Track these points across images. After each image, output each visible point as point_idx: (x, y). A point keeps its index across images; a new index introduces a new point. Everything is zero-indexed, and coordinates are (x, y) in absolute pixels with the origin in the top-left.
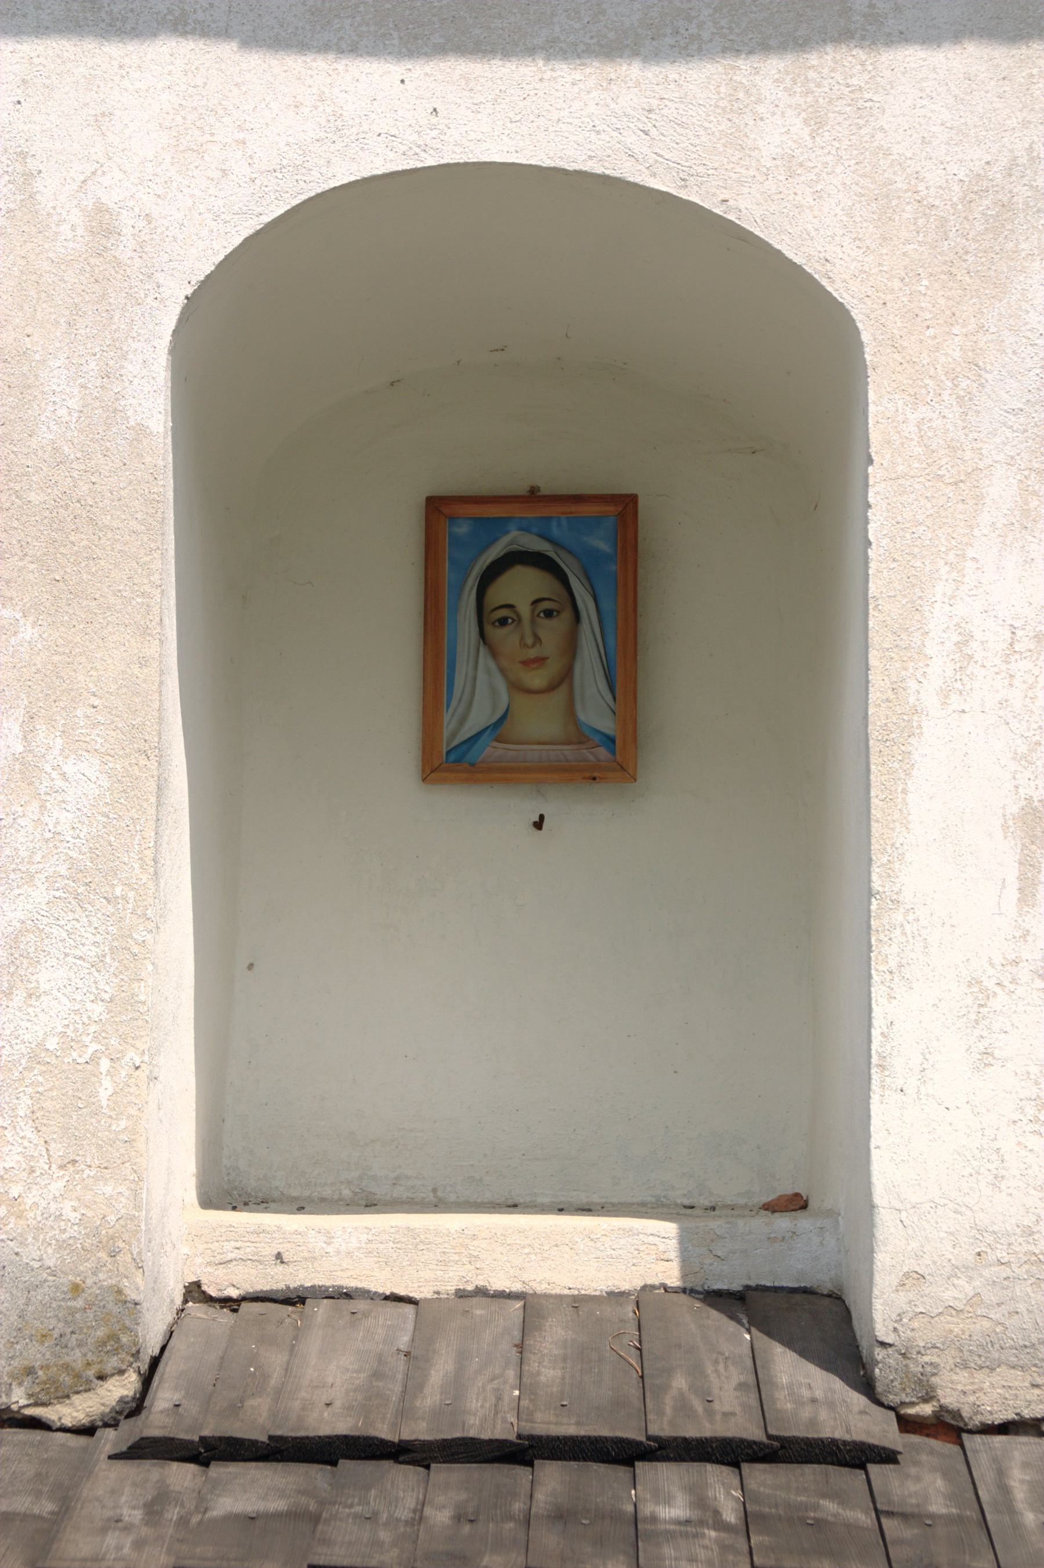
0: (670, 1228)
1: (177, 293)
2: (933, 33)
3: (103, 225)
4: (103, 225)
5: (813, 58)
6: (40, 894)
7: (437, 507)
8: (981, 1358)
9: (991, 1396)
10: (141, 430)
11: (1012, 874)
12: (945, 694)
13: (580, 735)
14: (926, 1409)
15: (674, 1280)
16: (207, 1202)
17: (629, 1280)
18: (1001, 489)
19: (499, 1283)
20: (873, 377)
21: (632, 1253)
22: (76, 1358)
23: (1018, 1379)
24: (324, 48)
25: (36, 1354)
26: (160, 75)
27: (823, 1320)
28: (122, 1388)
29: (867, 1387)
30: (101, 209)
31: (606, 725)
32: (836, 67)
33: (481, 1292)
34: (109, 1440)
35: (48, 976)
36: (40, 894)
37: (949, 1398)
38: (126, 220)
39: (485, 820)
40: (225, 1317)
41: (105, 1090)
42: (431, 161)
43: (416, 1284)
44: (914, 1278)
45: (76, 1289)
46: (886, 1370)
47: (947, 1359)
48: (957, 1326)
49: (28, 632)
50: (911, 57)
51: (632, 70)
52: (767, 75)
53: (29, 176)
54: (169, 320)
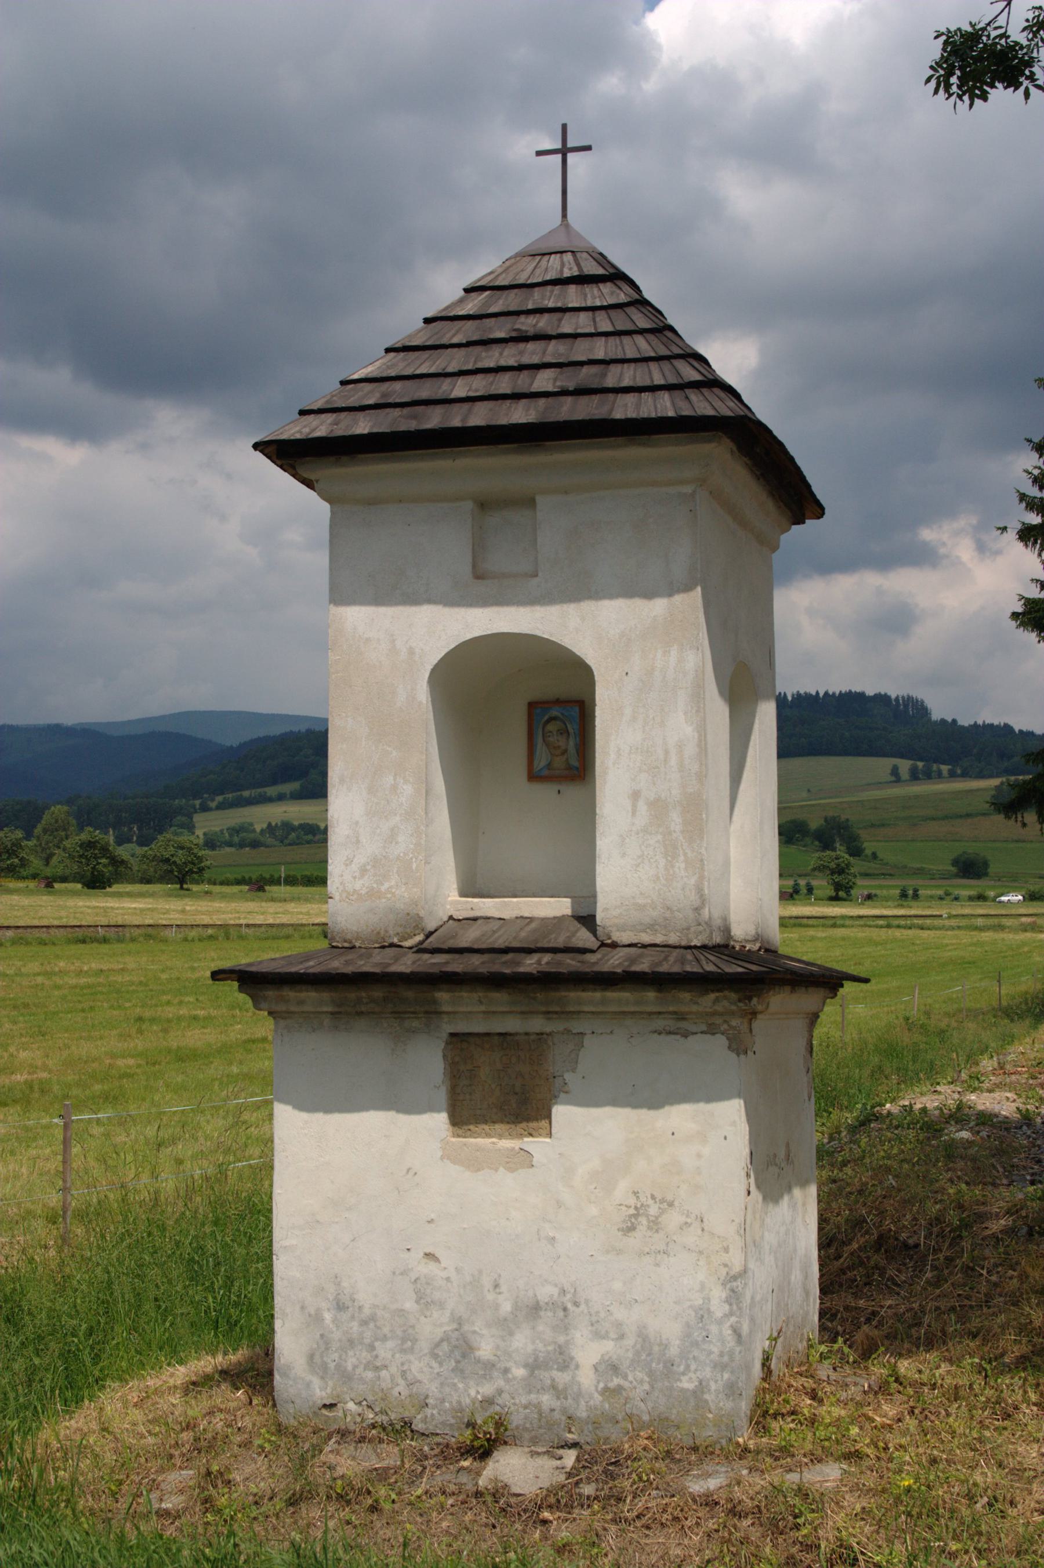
0: (569, 900)
1: (429, 668)
2: (611, 596)
3: (411, 651)
4: (411, 651)
5: (582, 604)
6: (398, 818)
7: (532, 705)
8: (623, 928)
9: (625, 938)
10: (421, 703)
11: (630, 809)
12: (614, 764)
13: (569, 767)
14: (609, 941)
15: (570, 913)
16: (463, 894)
17: (558, 914)
18: (628, 711)
19: (526, 915)
20: (597, 684)
21: (560, 907)
22: (408, 930)
23: (629, 933)
24: (463, 606)
25: (399, 930)
26: (425, 613)
27: (588, 921)
28: (420, 938)
29: (595, 935)
30: (411, 648)
31: (576, 764)
32: (588, 606)
33: (522, 917)
34: (415, 949)
35: (400, 838)
36: (398, 818)
37: (615, 938)
38: (417, 650)
39: (545, 792)
40: (456, 924)
41: (414, 866)
42: (489, 632)
43: (506, 915)
44: (606, 910)
45: (408, 914)
46: (600, 931)
47: (614, 929)
48: (616, 921)
49: (394, 753)
50: (606, 603)
51: (538, 608)
52: (571, 608)
53: (394, 641)
54: (427, 675)
